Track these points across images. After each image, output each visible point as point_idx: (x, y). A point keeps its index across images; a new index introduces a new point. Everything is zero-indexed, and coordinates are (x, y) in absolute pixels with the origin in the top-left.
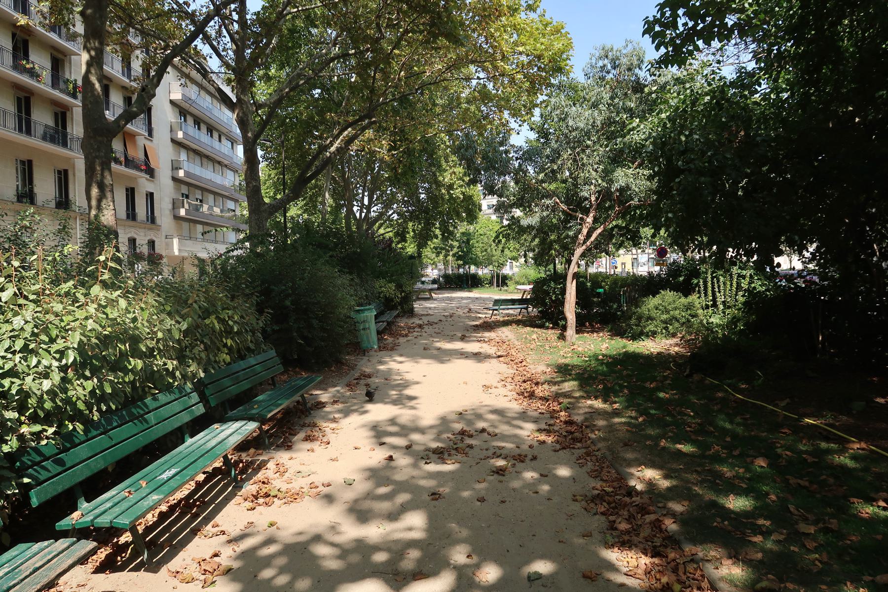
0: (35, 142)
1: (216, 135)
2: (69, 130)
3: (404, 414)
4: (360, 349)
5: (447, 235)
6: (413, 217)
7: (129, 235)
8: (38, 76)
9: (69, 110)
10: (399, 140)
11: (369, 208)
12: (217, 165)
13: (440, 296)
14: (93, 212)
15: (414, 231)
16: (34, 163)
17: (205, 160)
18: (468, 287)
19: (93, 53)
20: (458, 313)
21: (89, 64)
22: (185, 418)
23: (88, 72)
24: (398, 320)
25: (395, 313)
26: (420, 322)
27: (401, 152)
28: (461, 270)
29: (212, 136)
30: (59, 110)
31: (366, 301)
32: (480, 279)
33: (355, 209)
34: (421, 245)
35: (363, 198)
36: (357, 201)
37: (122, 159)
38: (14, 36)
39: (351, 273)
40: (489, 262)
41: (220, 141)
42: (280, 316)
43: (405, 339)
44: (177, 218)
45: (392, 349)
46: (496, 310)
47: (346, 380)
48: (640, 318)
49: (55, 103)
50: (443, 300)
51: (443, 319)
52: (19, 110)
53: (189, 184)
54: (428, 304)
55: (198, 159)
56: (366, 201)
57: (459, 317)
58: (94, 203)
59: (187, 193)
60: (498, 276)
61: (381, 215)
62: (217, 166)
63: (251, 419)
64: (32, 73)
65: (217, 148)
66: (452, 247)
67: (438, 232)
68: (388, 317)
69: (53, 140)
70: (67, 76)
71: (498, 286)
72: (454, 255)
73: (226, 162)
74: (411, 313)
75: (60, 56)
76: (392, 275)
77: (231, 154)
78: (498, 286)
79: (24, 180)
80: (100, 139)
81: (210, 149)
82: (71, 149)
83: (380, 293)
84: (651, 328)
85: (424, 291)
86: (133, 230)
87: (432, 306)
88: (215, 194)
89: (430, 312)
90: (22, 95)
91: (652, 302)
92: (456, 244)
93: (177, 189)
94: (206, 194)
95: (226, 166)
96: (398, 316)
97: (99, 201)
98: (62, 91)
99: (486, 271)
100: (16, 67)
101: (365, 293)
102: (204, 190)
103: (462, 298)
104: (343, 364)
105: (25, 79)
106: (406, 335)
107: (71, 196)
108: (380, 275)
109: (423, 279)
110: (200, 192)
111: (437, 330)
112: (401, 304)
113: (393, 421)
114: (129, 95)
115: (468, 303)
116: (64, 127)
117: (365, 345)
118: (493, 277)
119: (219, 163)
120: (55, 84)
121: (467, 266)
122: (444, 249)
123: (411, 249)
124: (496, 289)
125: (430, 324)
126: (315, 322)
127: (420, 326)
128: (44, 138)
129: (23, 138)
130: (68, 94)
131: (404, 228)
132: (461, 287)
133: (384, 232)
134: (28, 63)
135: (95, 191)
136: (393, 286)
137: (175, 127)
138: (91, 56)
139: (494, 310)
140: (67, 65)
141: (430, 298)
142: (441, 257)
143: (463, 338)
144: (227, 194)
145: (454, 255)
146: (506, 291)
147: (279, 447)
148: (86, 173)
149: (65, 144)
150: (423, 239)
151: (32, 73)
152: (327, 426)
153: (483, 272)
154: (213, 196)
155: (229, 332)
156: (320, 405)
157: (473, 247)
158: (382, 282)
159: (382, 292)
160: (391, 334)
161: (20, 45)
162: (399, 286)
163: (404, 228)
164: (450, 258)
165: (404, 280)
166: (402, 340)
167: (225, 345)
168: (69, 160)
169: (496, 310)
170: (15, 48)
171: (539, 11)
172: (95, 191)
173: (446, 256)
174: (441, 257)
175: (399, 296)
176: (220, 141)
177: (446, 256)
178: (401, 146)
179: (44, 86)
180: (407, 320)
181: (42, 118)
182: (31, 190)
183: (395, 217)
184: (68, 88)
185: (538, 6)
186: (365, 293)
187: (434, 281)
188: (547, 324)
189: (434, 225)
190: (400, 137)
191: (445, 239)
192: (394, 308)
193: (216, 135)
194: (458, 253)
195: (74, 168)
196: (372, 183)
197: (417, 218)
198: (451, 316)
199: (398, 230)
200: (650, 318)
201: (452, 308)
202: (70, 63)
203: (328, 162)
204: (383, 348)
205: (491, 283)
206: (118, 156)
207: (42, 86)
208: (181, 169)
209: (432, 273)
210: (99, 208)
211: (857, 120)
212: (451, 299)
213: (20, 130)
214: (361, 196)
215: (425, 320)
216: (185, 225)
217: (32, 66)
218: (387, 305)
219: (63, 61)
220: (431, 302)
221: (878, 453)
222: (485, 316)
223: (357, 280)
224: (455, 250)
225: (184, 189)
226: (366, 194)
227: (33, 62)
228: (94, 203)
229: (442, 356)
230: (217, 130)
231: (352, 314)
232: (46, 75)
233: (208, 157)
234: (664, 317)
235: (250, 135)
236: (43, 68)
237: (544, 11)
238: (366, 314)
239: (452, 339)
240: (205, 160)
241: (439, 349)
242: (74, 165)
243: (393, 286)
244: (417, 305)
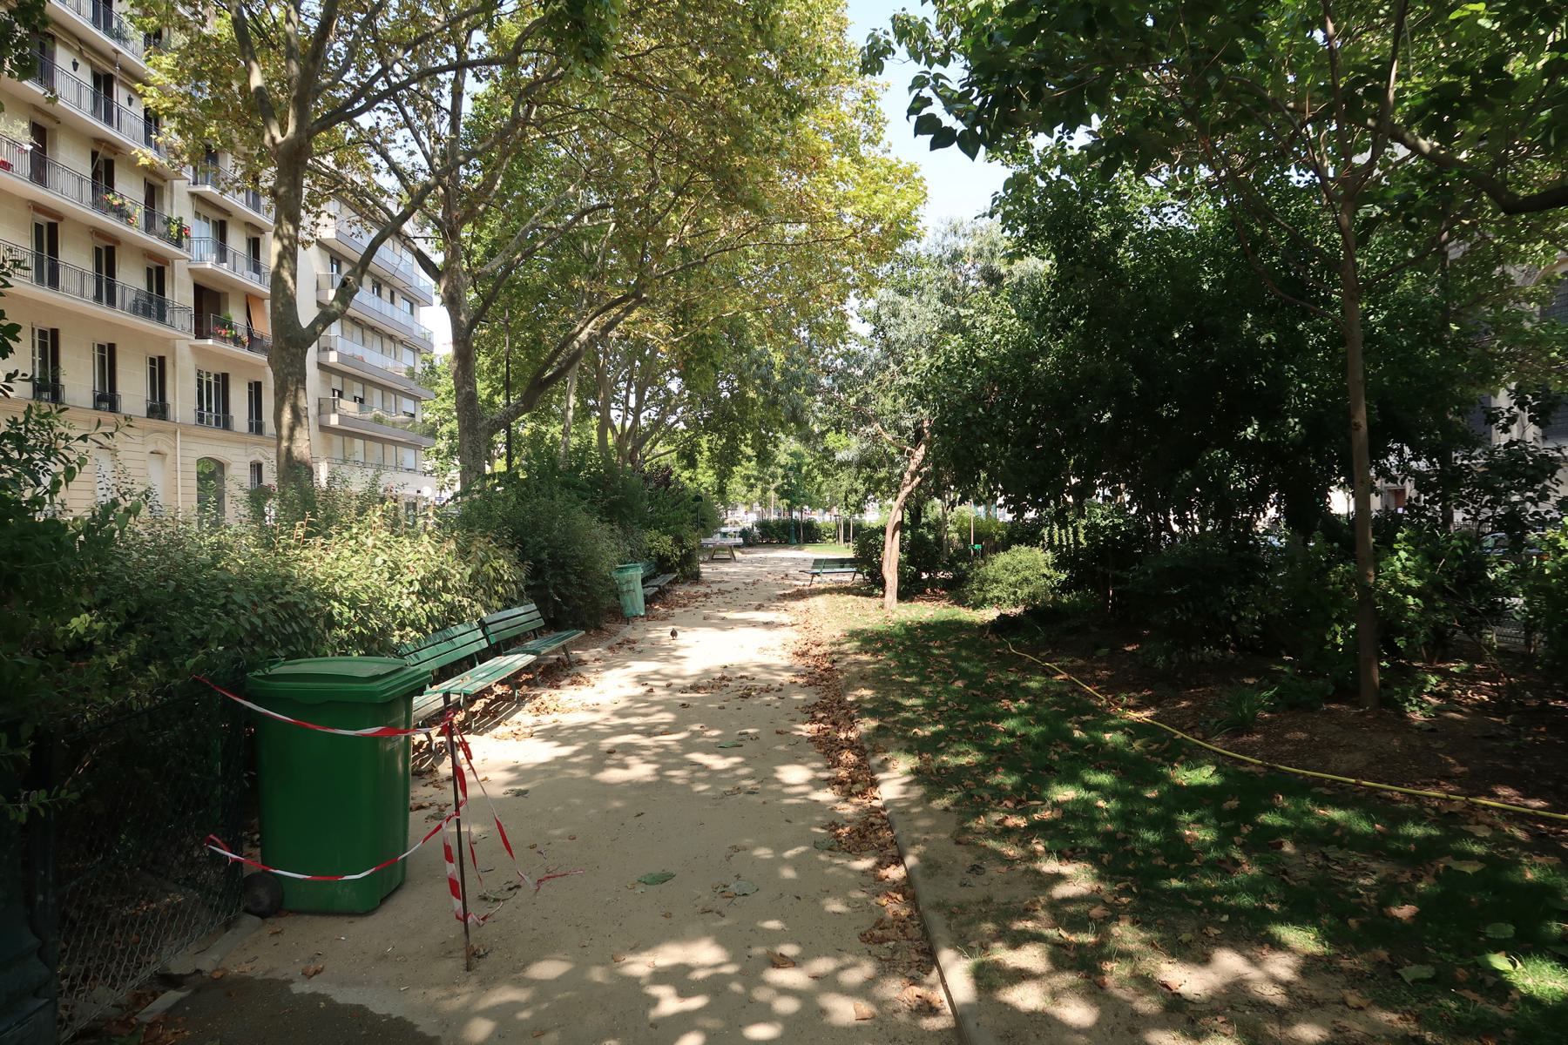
0: (120, 316)
1: (386, 292)
2: (168, 295)
3: (668, 668)
4: (621, 615)
5: (764, 458)
6: (710, 426)
7: (252, 458)
8: (128, 216)
9: (168, 264)
10: (682, 323)
11: (637, 412)
12: (387, 342)
13: (749, 556)
14: (285, 444)
15: (710, 449)
16: (118, 349)
17: (368, 334)
18: (799, 543)
19: (286, 242)
20: (765, 580)
21: (281, 257)
22: (475, 648)
23: (280, 265)
24: (676, 587)
25: (671, 577)
26: (708, 590)
27: (685, 339)
29: (379, 295)
30: (153, 264)
31: (634, 558)
33: (614, 414)
34: (724, 475)
35: (627, 397)
36: (617, 401)
37: (245, 338)
38: (94, 155)
39: (611, 522)
41: (392, 302)
42: (536, 573)
43: (682, 610)
44: (325, 429)
45: (664, 619)
46: (817, 574)
47: (609, 643)
48: (983, 581)
49: (149, 254)
50: (751, 561)
51: (742, 587)
52: (98, 269)
53: (343, 375)
54: (725, 568)
55: (357, 332)
56: (632, 403)
57: (766, 584)
58: (285, 432)
60: (847, 525)
61: (656, 425)
62: (388, 344)
63: (528, 652)
64: (121, 212)
65: (388, 314)
68: (661, 581)
69: (147, 313)
70: (167, 213)
71: (845, 541)
72: (776, 490)
73: (401, 336)
74: (696, 578)
75: (158, 182)
76: (668, 525)
77: (409, 324)
79: (43, 363)
80: (294, 350)
81: (376, 316)
82: (172, 326)
83: (650, 549)
84: (996, 593)
85: (722, 548)
86: (259, 449)
87: (733, 570)
88: (384, 388)
89: (726, 578)
90: (102, 244)
91: (1002, 558)
93: (327, 382)
94: (369, 388)
95: (402, 342)
96: (675, 582)
97: (292, 429)
98: (161, 237)
99: (827, 517)
100: (97, 204)
101: (629, 549)
102: (365, 382)
103: (782, 560)
104: (602, 629)
105: (110, 222)
106: (685, 605)
107: (169, 399)
108: (649, 524)
109: (723, 530)
110: (360, 386)
111: (728, 600)
112: (680, 564)
113: (656, 672)
114: (255, 235)
115: (788, 567)
116: (161, 291)
117: (629, 611)
118: (838, 526)
119: (391, 337)
120: (149, 227)
122: (761, 479)
123: (706, 477)
124: (843, 545)
125: (721, 592)
126: (573, 578)
127: (706, 595)
128: (135, 310)
129: (103, 311)
130: (170, 241)
131: (694, 446)
133: (662, 453)
134: (115, 198)
135: (287, 416)
136: (669, 539)
137: (324, 283)
138: (284, 247)
139: (814, 574)
140: (167, 194)
141: (732, 559)
142: (758, 492)
143: (759, 608)
144: (402, 388)
145: (776, 490)
147: (551, 687)
148: (276, 394)
149: (161, 317)
150: (726, 461)
151: (121, 212)
152: (592, 677)
153: (820, 518)
154: (379, 392)
155: (499, 580)
156: (581, 662)
158: (654, 533)
160: (664, 604)
161: (102, 169)
162: (678, 540)
163: (694, 446)
164: (772, 494)
165: (686, 530)
166: (677, 611)
167: (496, 592)
168: (167, 342)
169: (817, 574)
170: (95, 175)
171: (882, 145)
172: (287, 416)
173: (765, 491)
174: (758, 492)
176: (392, 302)
177: (765, 491)
178: (685, 330)
179: (135, 231)
180: (689, 589)
181: (131, 279)
182: (56, 379)
183: (681, 426)
184: (169, 231)
185: (881, 138)
186: (629, 549)
187: (744, 534)
188: (876, 591)
190: (683, 313)
192: (671, 570)
193: (386, 292)
194: (782, 486)
195: (174, 354)
196: (642, 374)
197: (716, 429)
198: (754, 584)
199: (685, 447)
200: (997, 581)
201: (761, 574)
202: (172, 191)
203: (577, 355)
204: (650, 616)
205: (836, 537)
206: (239, 334)
207: (134, 232)
208: (331, 349)
209: (743, 517)
210: (291, 438)
212: (763, 561)
213: (39, 279)
214: (624, 393)
215: (715, 588)
216: (337, 440)
217: (120, 201)
218: (661, 565)
219: (161, 188)
220: (732, 564)
221: (1082, 681)
222: (803, 583)
223: (619, 532)
224: (779, 481)
225: (336, 382)
226: (633, 390)
227: (121, 196)
228: (285, 432)
229: (725, 624)
230: (387, 284)
231: (614, 574)
232: (139, 213)
233: (373, 329)
234: (1012, 579)
235: (463, 318)
236: (135, 204)
237: (890, 145)
238: (631, 572)
239: (744, 608)
240: (368, 335)
241: (723, 619)
242: (174, 349)
243: (669, 539)
244: (706, 570)
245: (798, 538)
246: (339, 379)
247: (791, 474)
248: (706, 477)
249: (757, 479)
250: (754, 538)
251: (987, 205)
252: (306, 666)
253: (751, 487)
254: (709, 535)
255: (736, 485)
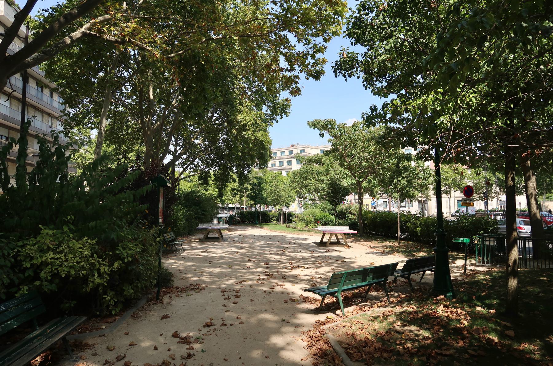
28: (253, 209)
32: (269, 216)
34: (221, 187)
40: (276, 201)
59: (7, 136)
66: (246, 189)
67: (235, 176)
71: (284, 222)
78: (284, 222)
83: (38, 269)
92: (250, 187)
94: (11, 131)
103: (254, 237)
119: (49, 114)
121: (258, 205)
123: (213, 191)
132: (252, 222)
142: (238, 198)
145: (248, 196)
146: (295, 228)
153: (273, 210)
157: (263, 189)
159: (45, 264)
164: (244, 199)
173: (241, 197)
174: (238, 198)
175: (105, 269)
177: (241, 197)
189: (231, 169)
191: (241, 183)
205: (278, 219)
211: (542, 100)
212: (242, 239)
245: (258, 220)
246: (7, 130)
247: (256, 187)
248: (213, 191)
249: (238, 191)
250: (236, 220)
251: (271, 148)
252: (198, 227)
253: (234, 195)
254: (210, 221)
255: (228, 194)
